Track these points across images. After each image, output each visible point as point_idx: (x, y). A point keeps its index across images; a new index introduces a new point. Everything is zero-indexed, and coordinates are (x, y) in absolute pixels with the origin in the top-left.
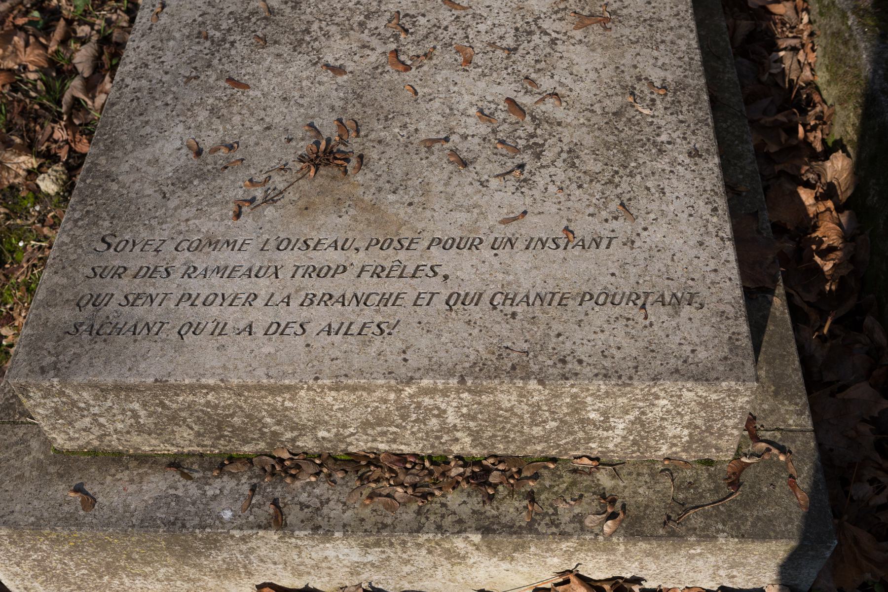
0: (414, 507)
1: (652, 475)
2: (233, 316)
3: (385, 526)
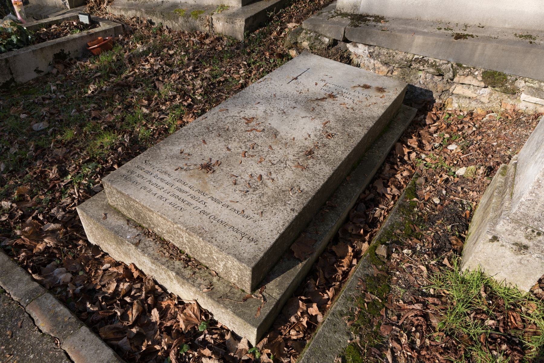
0: (167, 259)
1: (227, 286)
2: (155, 190)
3: (157, 259)
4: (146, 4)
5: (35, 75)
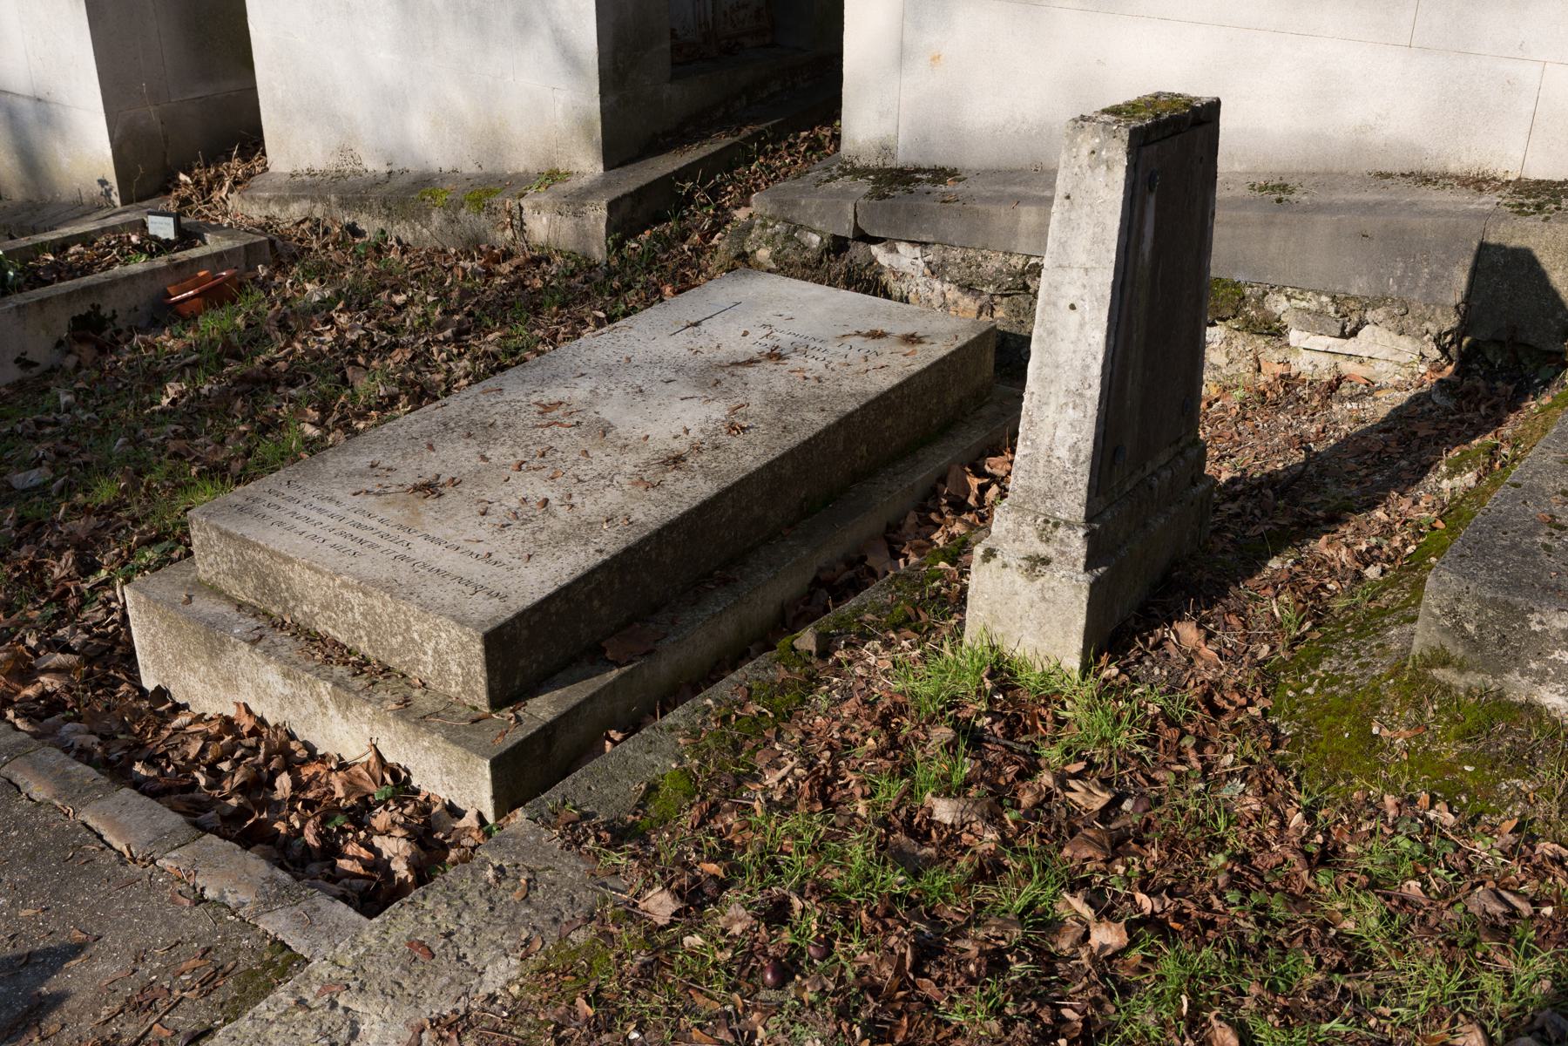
4: (343, 181)
5: (15, 373)
